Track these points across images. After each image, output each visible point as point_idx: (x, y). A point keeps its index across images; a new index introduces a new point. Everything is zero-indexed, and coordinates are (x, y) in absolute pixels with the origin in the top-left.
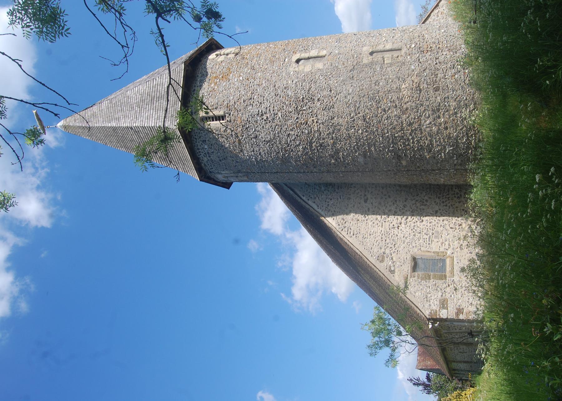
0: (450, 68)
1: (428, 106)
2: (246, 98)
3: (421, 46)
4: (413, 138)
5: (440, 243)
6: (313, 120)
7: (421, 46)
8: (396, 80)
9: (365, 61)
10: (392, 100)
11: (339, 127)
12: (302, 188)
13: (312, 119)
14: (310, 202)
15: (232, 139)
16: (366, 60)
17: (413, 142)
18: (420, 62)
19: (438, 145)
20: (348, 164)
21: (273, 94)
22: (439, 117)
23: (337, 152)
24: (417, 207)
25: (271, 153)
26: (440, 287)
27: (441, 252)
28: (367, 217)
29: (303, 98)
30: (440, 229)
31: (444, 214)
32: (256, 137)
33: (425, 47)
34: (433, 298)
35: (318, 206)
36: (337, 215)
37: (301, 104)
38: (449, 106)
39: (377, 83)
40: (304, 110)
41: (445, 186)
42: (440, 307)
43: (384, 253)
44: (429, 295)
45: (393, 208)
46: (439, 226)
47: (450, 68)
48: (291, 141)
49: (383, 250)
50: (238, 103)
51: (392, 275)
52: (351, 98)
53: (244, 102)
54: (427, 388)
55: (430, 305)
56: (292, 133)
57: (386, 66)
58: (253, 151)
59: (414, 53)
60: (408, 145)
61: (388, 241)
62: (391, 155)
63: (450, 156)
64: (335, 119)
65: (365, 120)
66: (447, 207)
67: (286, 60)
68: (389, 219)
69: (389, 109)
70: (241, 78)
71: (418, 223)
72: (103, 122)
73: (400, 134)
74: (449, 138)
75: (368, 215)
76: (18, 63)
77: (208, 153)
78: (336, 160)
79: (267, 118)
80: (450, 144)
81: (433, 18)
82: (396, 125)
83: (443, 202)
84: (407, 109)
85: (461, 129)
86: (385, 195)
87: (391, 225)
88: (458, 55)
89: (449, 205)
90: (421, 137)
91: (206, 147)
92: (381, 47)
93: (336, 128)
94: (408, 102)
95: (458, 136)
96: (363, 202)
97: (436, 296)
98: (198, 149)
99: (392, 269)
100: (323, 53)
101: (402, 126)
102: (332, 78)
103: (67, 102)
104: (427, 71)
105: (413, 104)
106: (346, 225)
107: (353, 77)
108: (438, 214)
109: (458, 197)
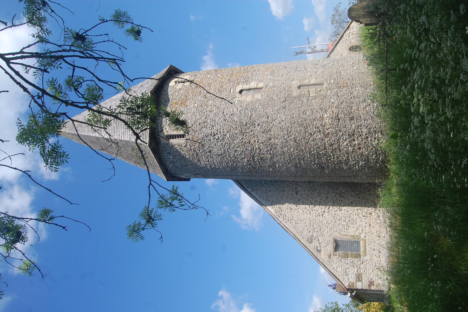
0: (362, 102)
1: (345, 132)
2: (201, 121)
3: (338, 81)
4: (334, 155)
5: (355, 228)
7: (338, 81)
8: (320, 110)
9: (295, 94)
10: (317, 126)
11: (275, 146)
13: (254, 139)
15: (191, 153)
16: (295, 93)
17: (334, 158)
18: (338, 96)
19: (353, 160)
21: (222, 119)
22: (354, 140)
23: (274, 163)
24: (337, 199)
25: (222, 163)
26: (356, 264)
27: (357, 236)
28: (298, 207)
29: (246, 123)
31: (358, 205)
32: (210, 152)
33: (342, 83)
34: (351, 272)
36: (275, 205)
37: (245, 128)
38: (362, 132)
39: (304, 112)
41: (358, 183)
42: (356, 280)
43: (312, 236)
44: (348, 271)
45: (318, 199)
46: (354, 214)
47: (362, 102)
48: (237, 155)
49: (311, 234)
51: (319, 254)
53: (199, 124)
55: (349, 278)
56: (239, 149)
57: (311, 98)
58: (208, 161)
59: (333, 88)
60: (330, 159)
61: (315, 226)
63: (363, 168)
64: (272, 140)
65: (295, 141)
66: (360, 199)
67: (232, 90)
68: (315, 208)
69: (314, 133)
70: (196, 105)
71: (338, 211)
72: (88, 132)
73: (323, 152)
74: (362, 155)
75: (299, 204)
76: (27, 174)
77: (173, 162)
78: (274, 169)
79: (218, 138)
80: (362, 159)
81: (345, 38)
83: (357, 195)
84: (328, 134)
85: (372, 149)
86: (312, 188)
87: (317, 213)
88: (368, 90)
90: (340, 155)
91: (171, 157)
92: (306, 82)
93: (273, 147)
94: (329, 128)
95: (368, 154)
97: (353, 271)
98: (165, 159)
99: (319, 249)
100: (261, 85)
101: (325, 146)
102: (268, 107)
103: (70, 202)
104: (344, 103)
105: (334, 130)
106: (282, 213)
107: (285, 107)
108: (354, 204)
109: (368, 191)
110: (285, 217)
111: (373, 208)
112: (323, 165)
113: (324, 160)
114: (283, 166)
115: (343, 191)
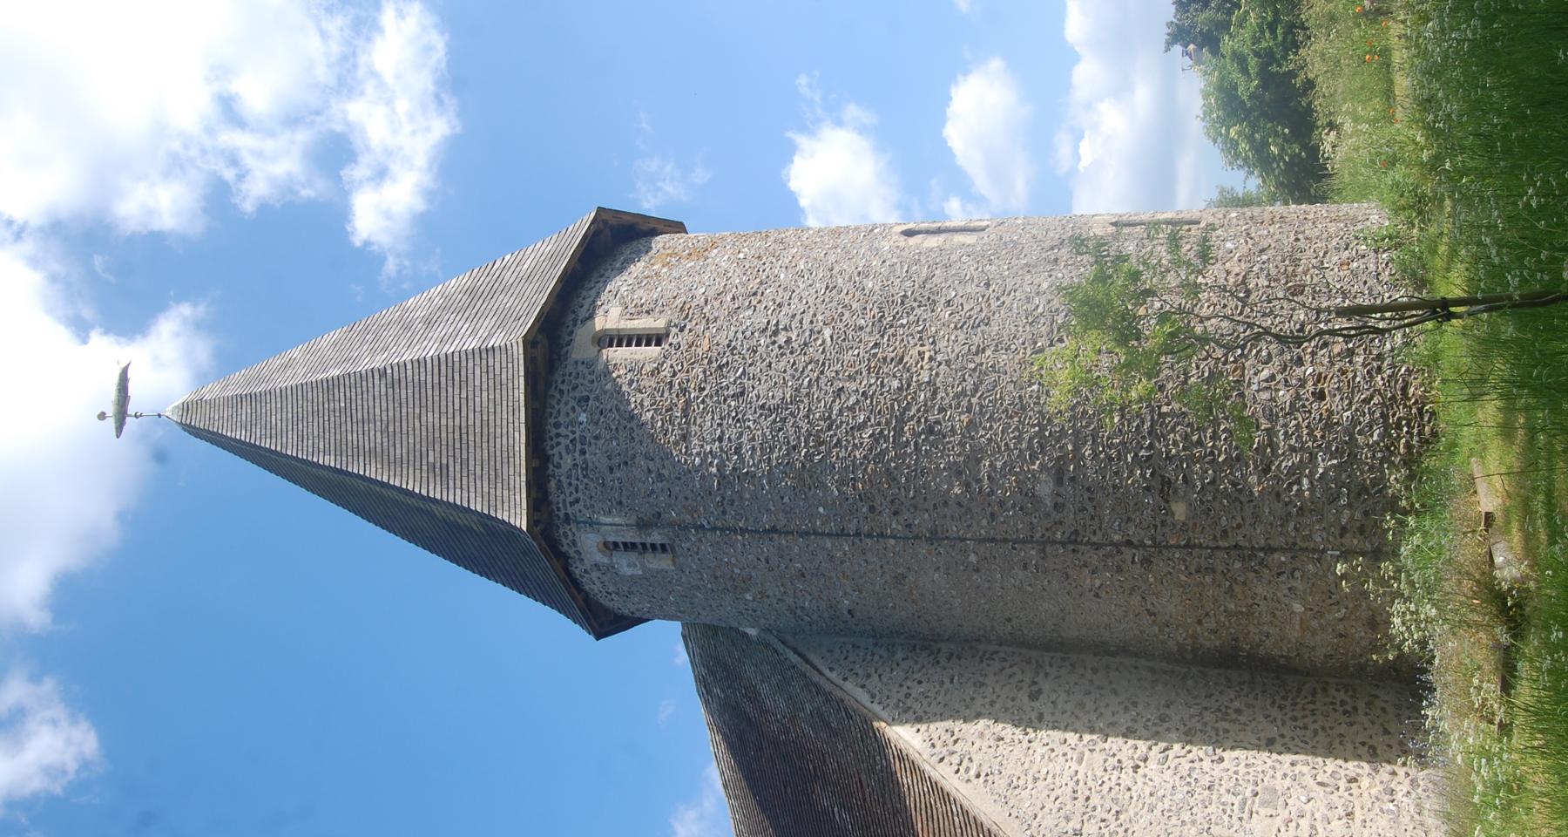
12: (831, 651)
14: (848, 686)
17: (1215, 437)
19: (1293, 449)
20: (1002, 503)
22: (1300, 362)
23: (975, 458)
24: (1205, 724)
30: (1280, 784)
35: (873, 696)
46: (1279, 775)
48: (841, 412)
50: (716, 304)
52: (1043, 302)
56: (852, 386)
58: (720, 439)
60: (1200, 443)
62: (1143, 475)
64: (988, 352)
66: (1309, 733)
68: (1107, 746)
71: (1206, 764)
74: (1329, 426)
77: (583, 440)
78: (967, 485)
79: (788, 341)
82: (1168, 378)
83: (1295, 719)
85: (1367, 401)
89: (1316, 726)
91: (583, 418)
95: (1355, 422)
96: (1026, 699)
98: (557, 425)
101: (1185, 382)
104: (1271, 252)
106: (957, 747)
108: (1278, 746)
109: (1345, 712)
110: (966, 763)
111: (1364, 764)
112: (1170, 473)
113: (1175, 443)
114: (1009, 467)
115: (1237, 704)
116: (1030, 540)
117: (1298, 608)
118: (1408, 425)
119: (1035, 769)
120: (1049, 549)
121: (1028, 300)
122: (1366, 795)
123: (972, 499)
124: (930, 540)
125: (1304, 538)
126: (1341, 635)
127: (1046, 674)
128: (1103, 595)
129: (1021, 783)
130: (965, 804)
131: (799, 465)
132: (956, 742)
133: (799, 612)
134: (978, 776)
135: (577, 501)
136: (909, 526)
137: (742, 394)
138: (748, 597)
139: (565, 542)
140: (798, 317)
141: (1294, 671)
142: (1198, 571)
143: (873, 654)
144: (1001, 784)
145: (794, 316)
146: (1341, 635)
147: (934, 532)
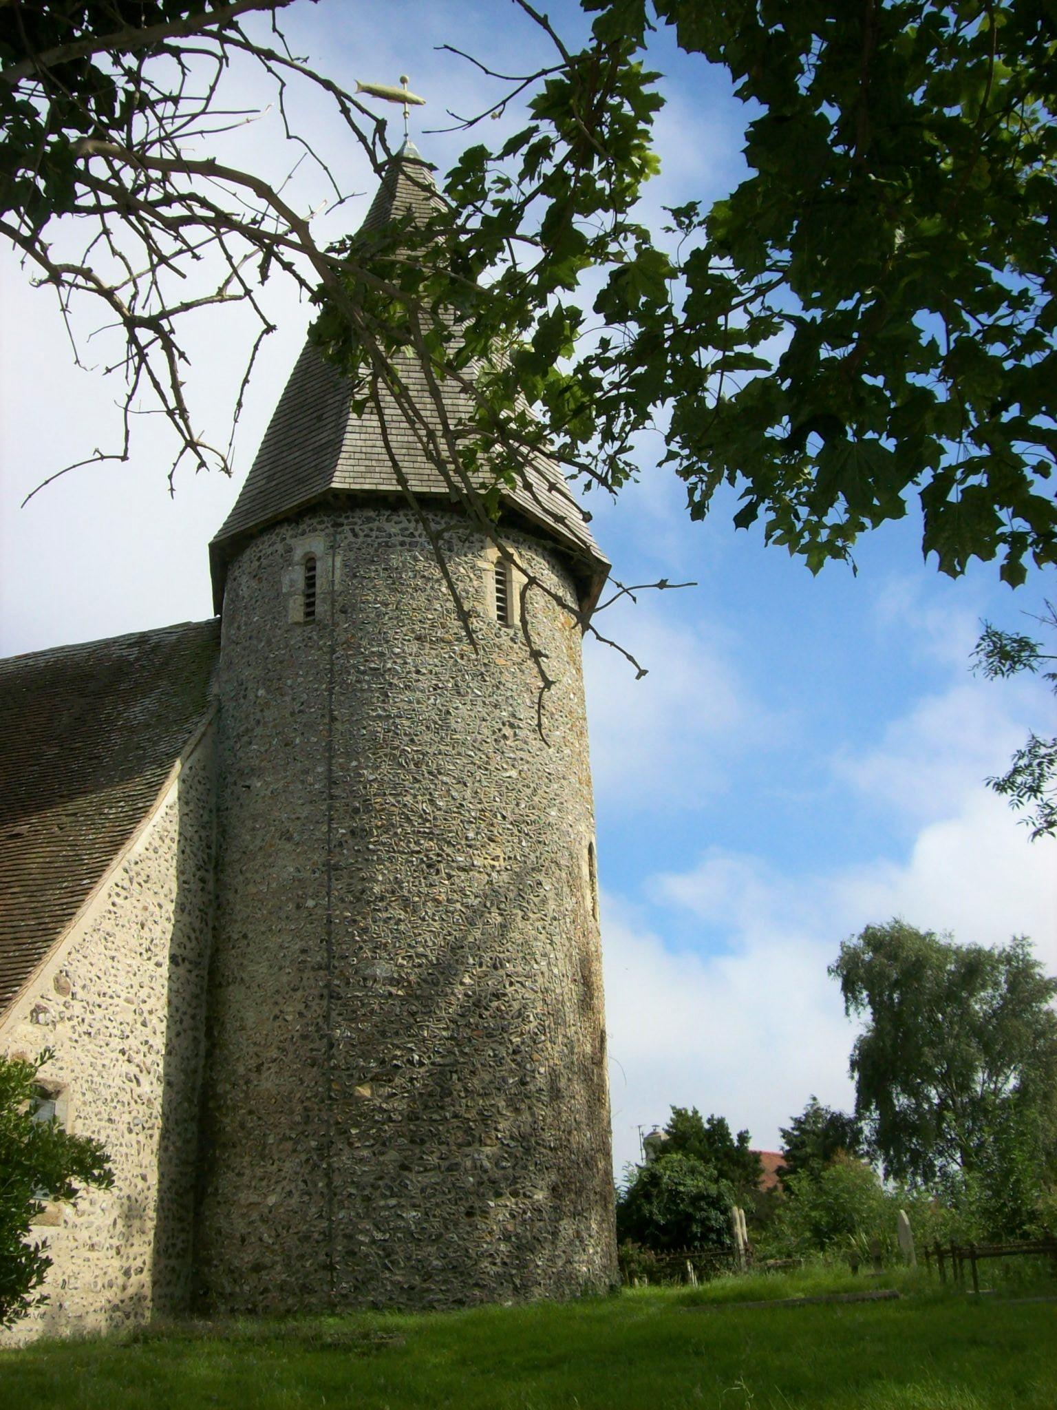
6: (495, 858)
40: (520, 842)
54: (868, 928)
56: (468, 794)
58: (418, 672)
69: (518, 1064)
79: (505, 737)
106: (135, 885)
110: (123, 893)
115: (171, 1148)
116: (331, 956)
117: (272, 1200)
118: (448, 1290)
119: (121, 958)
120: (322, 973)
121: (544, 955)
122: (107, 1263)
123: (369, 902)
124: (327, 864)
125: (341, 1201)
126: (243, 1240)
127: (190, 971)
128: (277, 1024)
129: (109, 944)
130: (93, 892)
131: (397, 743)
132: (140, 884)
133: (246, 739)
134: (114, 904)
135: (356, 535)
136: (341, 845)
137: (459, 693)
138: (261, 692)
139: (314, 521)
140: (525, 747)
141: (199, 1202)
142: (305, 1109)
143: (204, 808)
144: (108, 926)
145: (526, 743)
146: (243, 1240)
147: (336, 868)
